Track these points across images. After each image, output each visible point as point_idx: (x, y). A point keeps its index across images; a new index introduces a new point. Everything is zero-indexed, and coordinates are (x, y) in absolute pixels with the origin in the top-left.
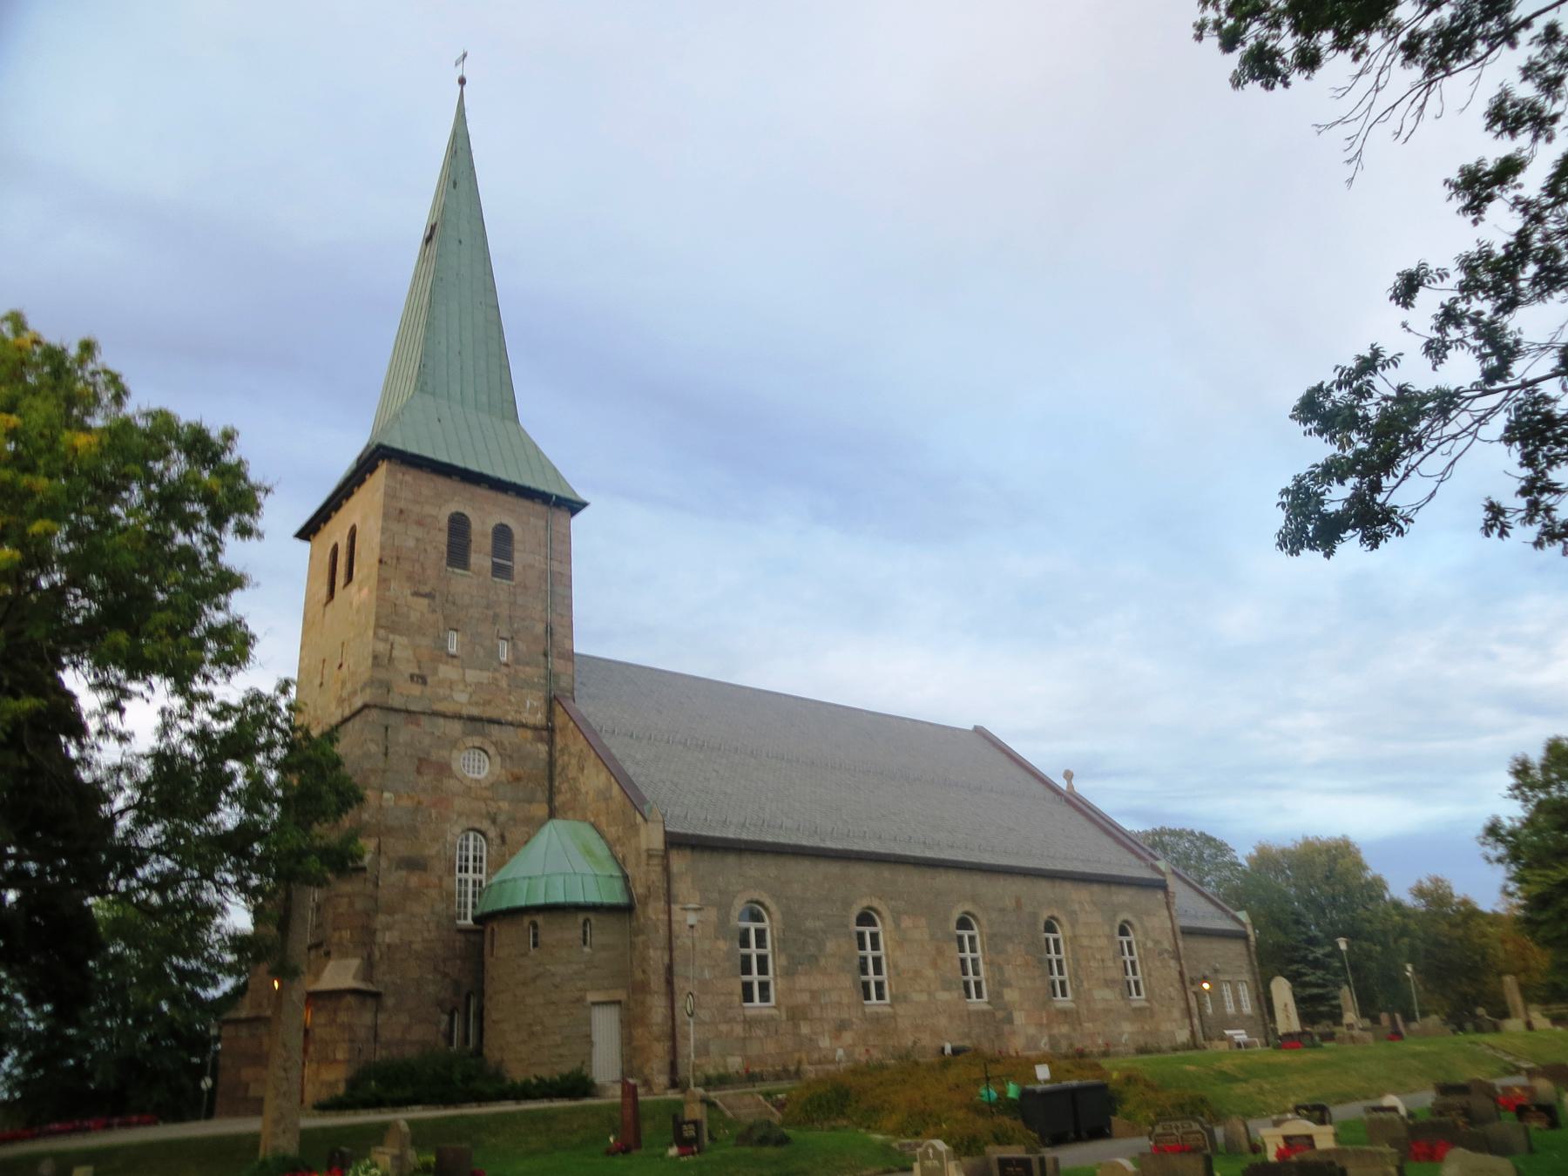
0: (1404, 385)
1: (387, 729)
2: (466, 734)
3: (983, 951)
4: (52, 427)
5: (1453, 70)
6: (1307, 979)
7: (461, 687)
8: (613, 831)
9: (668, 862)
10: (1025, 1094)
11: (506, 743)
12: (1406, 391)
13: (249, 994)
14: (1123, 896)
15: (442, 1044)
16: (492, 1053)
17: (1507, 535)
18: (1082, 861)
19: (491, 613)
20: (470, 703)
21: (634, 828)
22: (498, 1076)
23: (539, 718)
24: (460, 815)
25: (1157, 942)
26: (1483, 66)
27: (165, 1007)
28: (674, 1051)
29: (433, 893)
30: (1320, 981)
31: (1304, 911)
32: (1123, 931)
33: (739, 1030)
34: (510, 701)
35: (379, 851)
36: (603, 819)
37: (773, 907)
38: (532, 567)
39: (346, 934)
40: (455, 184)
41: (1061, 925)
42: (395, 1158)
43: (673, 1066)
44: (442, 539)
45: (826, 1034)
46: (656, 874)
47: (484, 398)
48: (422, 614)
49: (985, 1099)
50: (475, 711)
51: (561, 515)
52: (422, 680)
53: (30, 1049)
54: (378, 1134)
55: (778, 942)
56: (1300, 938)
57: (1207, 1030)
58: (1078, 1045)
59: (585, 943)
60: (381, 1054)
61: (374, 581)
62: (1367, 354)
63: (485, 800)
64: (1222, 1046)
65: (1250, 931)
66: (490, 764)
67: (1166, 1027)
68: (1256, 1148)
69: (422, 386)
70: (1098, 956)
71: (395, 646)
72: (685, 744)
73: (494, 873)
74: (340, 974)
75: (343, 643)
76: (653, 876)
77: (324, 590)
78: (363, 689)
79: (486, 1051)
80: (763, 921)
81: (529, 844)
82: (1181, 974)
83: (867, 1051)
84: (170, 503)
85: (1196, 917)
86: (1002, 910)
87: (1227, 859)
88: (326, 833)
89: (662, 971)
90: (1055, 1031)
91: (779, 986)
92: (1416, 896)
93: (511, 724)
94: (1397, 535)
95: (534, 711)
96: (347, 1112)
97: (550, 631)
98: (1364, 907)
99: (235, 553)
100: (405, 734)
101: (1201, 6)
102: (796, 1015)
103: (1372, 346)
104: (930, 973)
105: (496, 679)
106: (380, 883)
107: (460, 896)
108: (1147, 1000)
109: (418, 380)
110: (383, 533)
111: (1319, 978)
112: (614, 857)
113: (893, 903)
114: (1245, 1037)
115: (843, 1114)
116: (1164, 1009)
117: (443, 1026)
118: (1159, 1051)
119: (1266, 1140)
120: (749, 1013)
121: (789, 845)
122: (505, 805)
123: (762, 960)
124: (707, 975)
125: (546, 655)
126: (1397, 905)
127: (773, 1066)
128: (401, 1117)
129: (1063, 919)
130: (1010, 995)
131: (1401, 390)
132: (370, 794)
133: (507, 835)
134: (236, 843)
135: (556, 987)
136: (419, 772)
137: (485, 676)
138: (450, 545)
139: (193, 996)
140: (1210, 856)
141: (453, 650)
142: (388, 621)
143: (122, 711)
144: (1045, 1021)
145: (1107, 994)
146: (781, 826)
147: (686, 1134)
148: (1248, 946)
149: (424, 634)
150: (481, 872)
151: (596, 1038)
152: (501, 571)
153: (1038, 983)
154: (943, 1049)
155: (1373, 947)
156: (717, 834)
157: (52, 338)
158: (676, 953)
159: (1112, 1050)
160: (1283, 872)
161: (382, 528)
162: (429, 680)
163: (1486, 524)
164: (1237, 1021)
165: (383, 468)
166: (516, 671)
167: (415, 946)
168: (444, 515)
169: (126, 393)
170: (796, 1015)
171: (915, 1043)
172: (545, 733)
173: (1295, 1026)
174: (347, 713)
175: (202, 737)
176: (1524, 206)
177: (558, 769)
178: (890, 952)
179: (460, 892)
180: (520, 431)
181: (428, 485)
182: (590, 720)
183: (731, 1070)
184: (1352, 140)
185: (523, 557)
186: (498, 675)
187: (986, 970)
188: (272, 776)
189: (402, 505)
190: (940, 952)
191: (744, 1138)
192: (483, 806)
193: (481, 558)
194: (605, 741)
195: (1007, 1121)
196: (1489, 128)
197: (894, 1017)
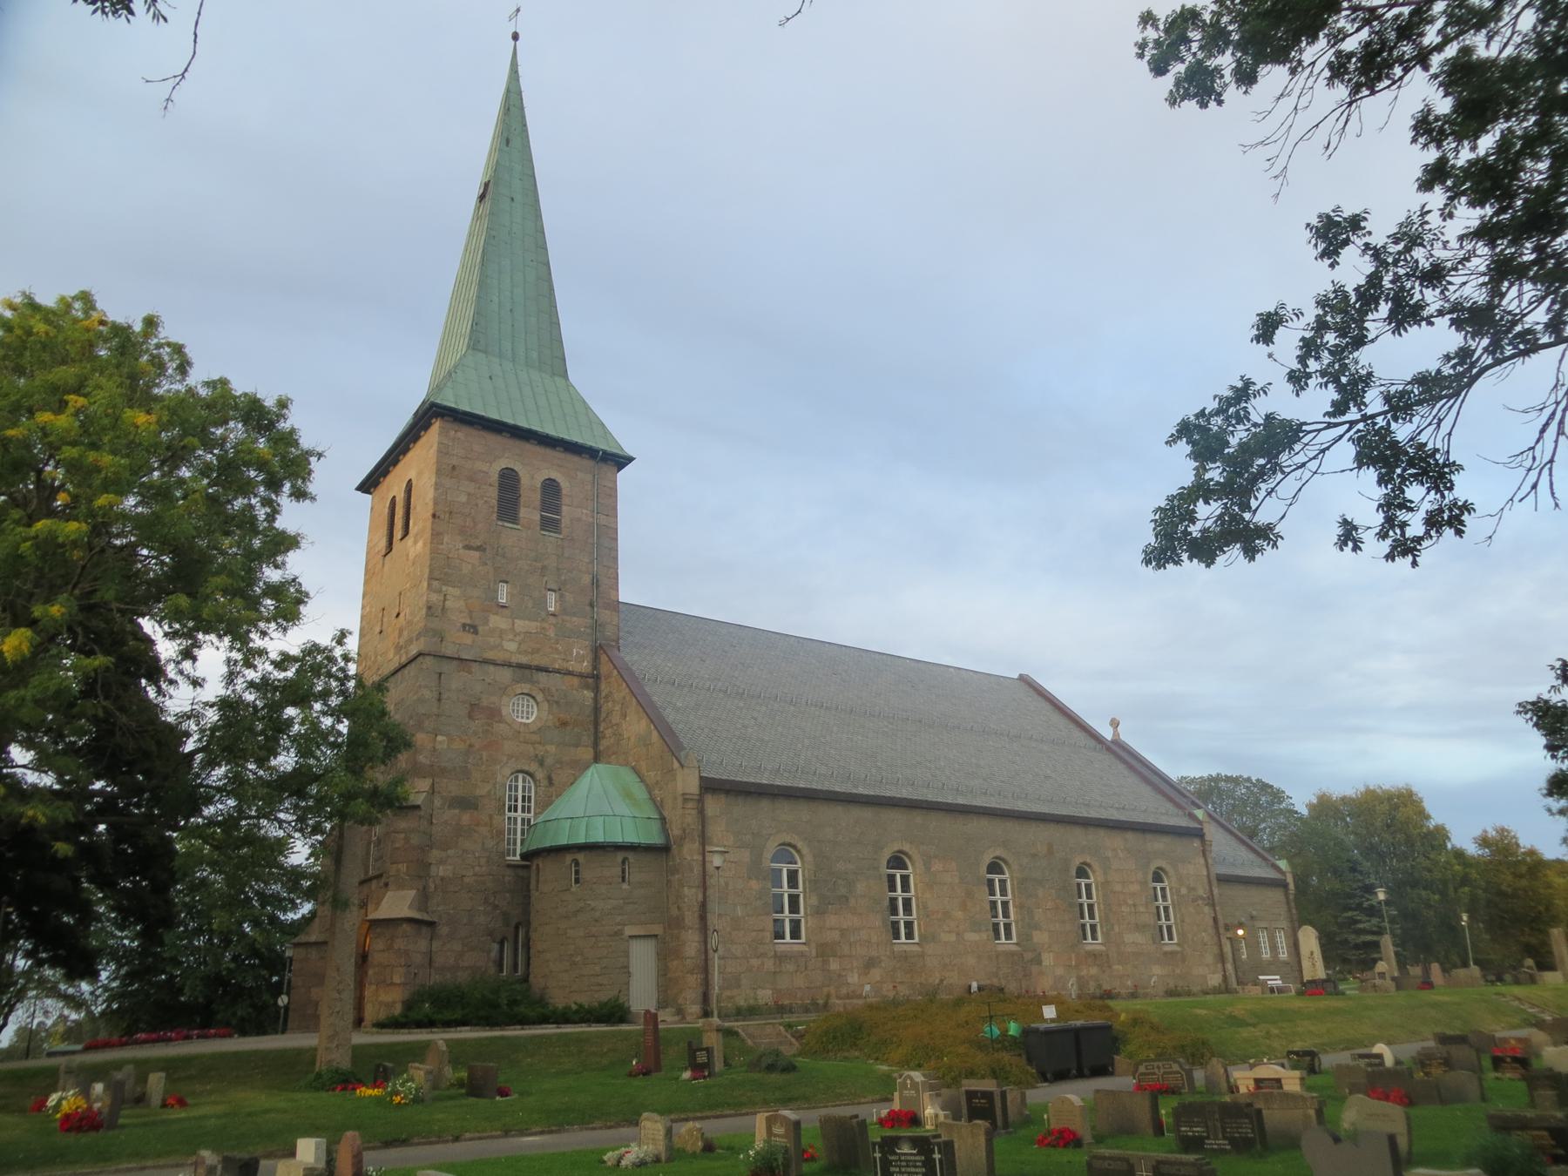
0: (1271, 414)
1: (440, 674)
4: (114, 407)
5: (1377, 89)
6: (1361, 926)
7: (511, 637)
8: (652, 776)
9: (703, 803)
10: (1026, 1032)
11: (554, 689)
12: (1274, 418)
13: (317, 920)
14: (1159, 844)
15: (492, 970)
16: (537, 981)
17: (1360, 549)
18: (1118, 809)
19: (539, 565)
22: (541, 1001)
23: (585, 666)
24: (510, 757)
25: (1191, 889)
26: (1399, 87)
27: (247, 928)
28: (706, 983)
29: (484, 830)
30: (1374, 929)
31: (1360, 858)
32: (1157, 878)
33: (769, 965)
34: (557, 649)
35: (433, 791)
36: (643, 765)
37: (805, 851)
38: (579, 520)
39: (403, 867)
41: (1094, 872)
43: (706, 998)
44: (493, 493)
45: (855, 971)
46: (691, 818)
47: (535, 355)
49: (988, 1035)
50: (524, 660)
51: (607, 469)
52: (474, 629)
54: (417, 1052)
55: (810, 882)
56: (1355, 886)
58: (1106, 987)
59: (623, 880)
60: (436, 978)
61: (428, 535)
62: (1239, 384)
66: (538, 710)
68: (1233, 1089)
69: (478, 341)
70: (1130, 902)
71: (448, 597)
72: (726, 692)
73: (540, 813)
74: (396, 904)
75: (400, 594)
77: (383, 543)
79: (531, 978)
80: (796, 863)
82: (1215, 920)
83: (894, 987)
84: (230, 474)
86: (1034, 856)
87: (1283, 805)
88: (379, 776)
89: (696, 909)
90: (1084, 973)
91: (809, 925)
92: (1480, 845)
93: (558, 672)
94: (1273, 548)
95: (580, 659)
96: (402, 1031)
97: (595, 582)
98: (1424, 856)
99: (291, 517)
100: (457, 680)
101: (1141, 27)
102: (826, 951)
103: (1242, 377)
104: (959, 914)
106: (434, 821)
107: (509, 834)
109: (470, 339)
110: (436, 489)
111: (1375, 926)
112: (652, 799)
115: (855, 1045)
117: (494, 954)
118: (1189, 994)
119: (1239, 1082)
120: (781, 948)
121: (821, 791)
122: (552, 749)
123: (794, 900)
124: (739, 912)
125: (592, 605)
126: (1459, 854)
128: (439, 1037)
129: (1096, 866)
130: (1040, 937)
131: (1269, 418)
132: (420, 738)
134: (294, 784)
136: (470, 716)
137: (533, 626)
138: (501, 500)
139: (273, 920)
140: (1267, 802)
142: (441, 572)
143: (194, 659)
145: (1139, 938)
147: (699, 1060)
148: (1287, 894)
150: (529, 812)
152: (550, 524)
154: (970, 987)
155: (1432, 895)
157: (116, 315)
158: (710, 892)
159: (1141, 991)
160: (1343, 820)
161: (436, 484)
162: (480, 629)
163: (1339, 539)
164: (1273, 966)
165: (436, 426)
166: (563, 621)
167: (466, 880)
169: (189, 364)
170: (826, 951)
171: (942, 981)
172: (590, 681)
173: (1321, 973)
174: (404, 660)
175: (263, 686)
176: (1377, 254)
177: (603, 715)
178: (920, 895)
179: (509, 829)
180: (569, 385)
183: (761, 1002)
184: (1272, 161)
186: (546, 625)
187: (1016, 913)
189: (454, 461)
191: (753, 1066)
193: (530, 512)
194: (647, 689)
195: (1006, 1057)
196: (1414, 141)
197: (922, 955)
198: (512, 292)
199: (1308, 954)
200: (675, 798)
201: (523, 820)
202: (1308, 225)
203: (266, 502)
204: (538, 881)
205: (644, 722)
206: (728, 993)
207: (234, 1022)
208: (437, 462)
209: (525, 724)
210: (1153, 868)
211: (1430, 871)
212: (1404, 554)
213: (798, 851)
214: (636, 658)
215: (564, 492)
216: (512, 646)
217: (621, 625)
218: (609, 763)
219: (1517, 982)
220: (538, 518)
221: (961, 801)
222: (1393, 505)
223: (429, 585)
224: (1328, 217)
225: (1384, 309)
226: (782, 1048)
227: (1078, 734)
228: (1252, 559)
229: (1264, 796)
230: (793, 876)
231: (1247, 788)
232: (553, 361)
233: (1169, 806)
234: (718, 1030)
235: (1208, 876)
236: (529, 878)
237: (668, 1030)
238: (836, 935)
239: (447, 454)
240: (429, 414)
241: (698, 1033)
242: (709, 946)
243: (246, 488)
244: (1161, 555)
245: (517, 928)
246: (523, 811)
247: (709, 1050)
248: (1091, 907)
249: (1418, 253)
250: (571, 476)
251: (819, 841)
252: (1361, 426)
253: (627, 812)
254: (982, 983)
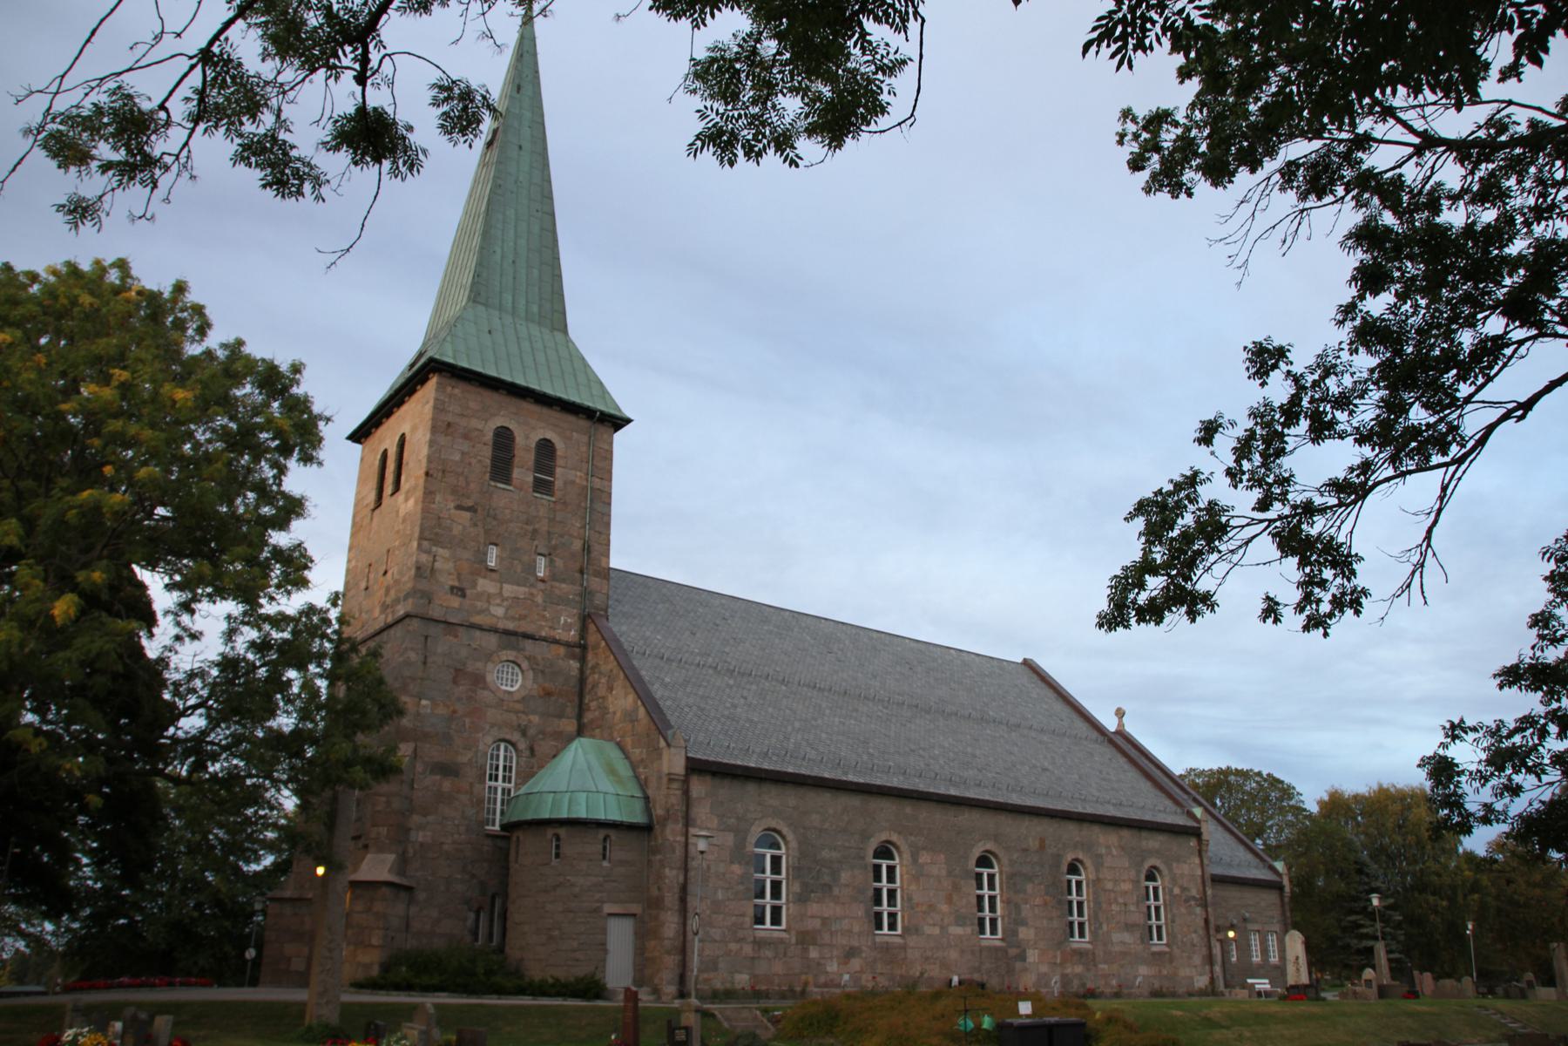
1: (426, 637)
2: (502, 647)
3: (1001, 889)
6: (1364, 931)
7: (498, 601)
8: (637, 753)
10: (1001, 1027)
11: (539, 657)
14: (1154, 842)
15: (468, 938)
16: (513, 952)
19: (530, 528)
21: (657, 753)
22: (517, 973)
23: (572, 635)
24: (493, 725)
25: (1183, 889)
27: (210, 877)
28: (684, 965)
33: (748, 949)
34: (544, 616)
36: (628, 740)
37: (790, 836)
38: (573, 482)
39: (384, 830)
40: (519, 88)
41: (1085, 868)
42: (422, 1032)
43: (682, 979)
44: (487, 453)
47: (535, 309)
48: (464, 527)
49: (962, 1028)
50: (511, 626)
51: (603, 430)
52: (460, 591)
53: (88, 905)
54: (409, 1012)
55: (794, 868)
56: (1361, 888)
57: (1228, 977)
58: (1090, 985)
59: (604, 857)
61: (419, 493)
62: (1189, 473)
63: (517, 712)
64: (1242, 994)
65: (1286, 882)
67: (1185, 972)
69: (479, 293)
70: (1121, 900)
73: (524, 783)
74: (376, 867)
76: (673, 800)
77: (372, 496)
78: (406, 598)
79: (507, 949)
81: (557, 759)
82: (1207, 921)
85: (1230, 865)
86: (1025, 850)
87: (1292, 802)
89: (676, 890)
90: (1069, 971)
93: (544, 639)
95: (567, 627)
97: (587, 548)
99: (297, 480)
100: (443, 644)
102: (806, 939)
104: (944, 908)
105: (532, 594)
107: (489, 803)
112: (637, 777)
113: (913, 838)
114: (1268, 986)
116: (1185, 954)
117: (470, 922)
118: (1174, 995)
121: (809, 777)
122: (535, 719)
123: (776, 886)
124: (720, 895)
125: (582, 572)
127: (779, 985)
128: (429, 1001)
129: (1088, 863)
130: (1025, 933)
133: (536, 748)
135: (575, 896)
136: (455, 682)
137: (521, 591)
138: (494, 459)
141: (492, 564)
142: (432, 532)
144: (1058, 961)
145: (1127, 937)
146: (804, 759)
149: (465, 548)
150: (510, 782)
151: (610, 946)
152: (542, 486)
153: (1055, 924)
154: (951, 981)
156: (739, 763)
157: (150, 284)
158: (691, 874)
159: (1125, 991)
160: (1355, 819)
162: (468, 592)
165: (433, 381)
167: (446, 847)
169: (209, 326)
170: (806, 939)
171: (922, 974)
174: (390, 619)
176: (1297, 379)
180: (568, 341)
181: (475, 398)
182: (622, 639)
183: (738, 987)
186: (534, 591)
187: (1002, 909)
188: (322, 684)
189: (450, 418)
190: (956, 888)
192: (514, 718)
193: (523, 474)
194: (635, 662)
197: (904, 947)
198: (515, 244)
199: (1293, 959)
200: (660, 778)
201: (503, 790)
202: (1245, 348)
203: (275, 465)
204: (517, 853)
205: (631, 697)
206: (706, 975)
207: (58, 989)
208: (433, 419)
209: (509, 693)
210: (1146, 866)
211: (1439, 875)
212: (1316, 626)
213: (783, 837)
214: (624, 628)
215: (559, 453)
216: (500, 611)
217: (611, 593)
218: (593, 737)
219: (1507, 996)
220: (530, 479)
221: (953, 792)
222: (1310, 583)
223: (419, 545)
224: (1261, 344)
225: (1304, 424)
226: (758, 1032)
227: (1080, 724)
228: (1193, 620)
229: (1274, 792)
230: (776, 861)
231: (1257, 782)
232: (554, 315)
233: (1168, 803)
234: (697, 1011)
235: (1203, 876)
236: (508, 850)
237: (646, 1008)
238: (817, 923)
239: (443, 410)
240: (424, 371)
241: (678, 1012)
242: (689, 928)
243: (258, 452)
244: (1114, 619)
245: (493, 897)
246: (504, 781)
247: (687, 1029)
248: (1080, 904)
249: (1331, 382)
250: (565, 436)
251: (804, 828)
252: (1278, 524)
253: (611, 789)
254: (963, 977)
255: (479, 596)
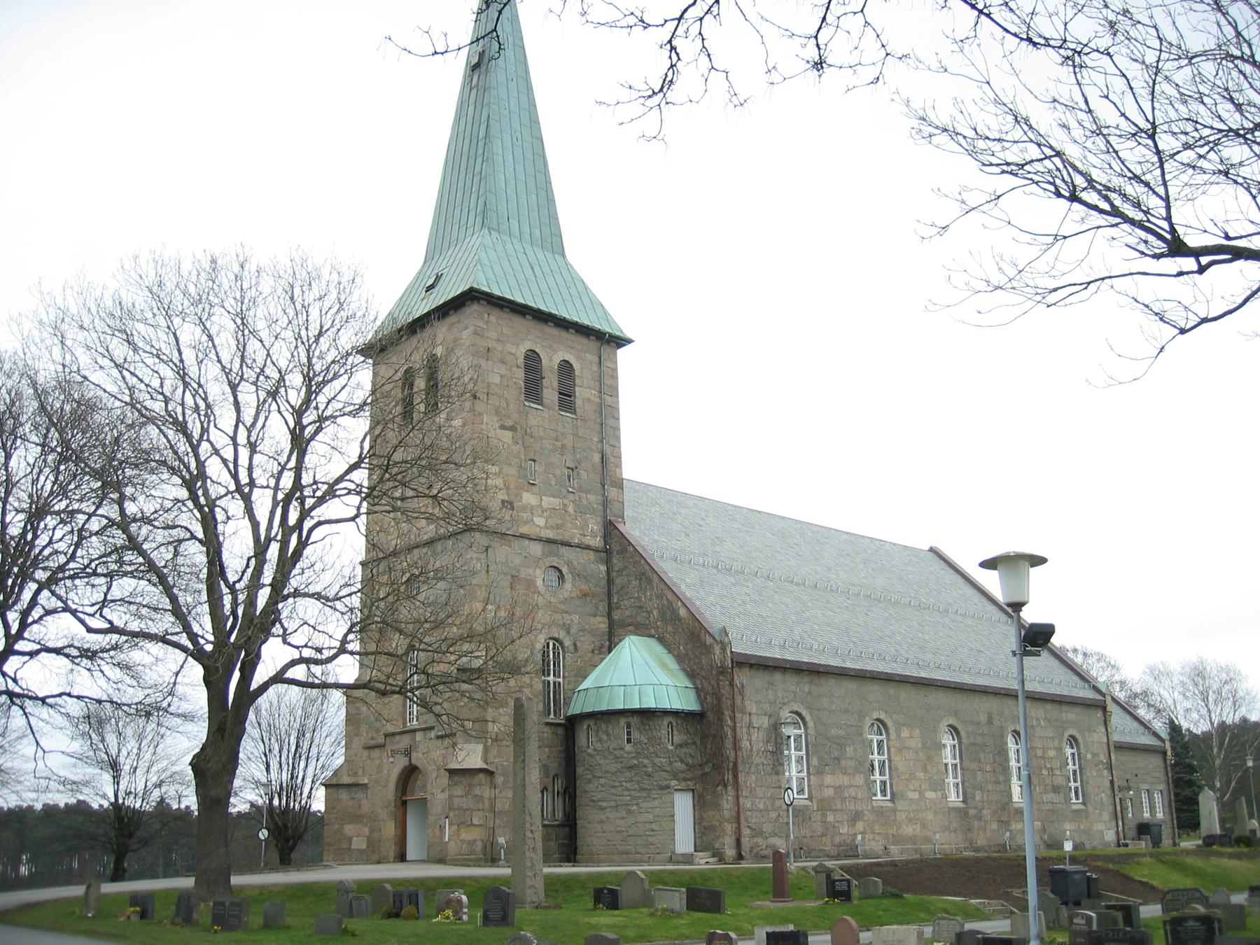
2: (545, 555)
11: (575, 563)
14: (1070, 714)
19: (559, 444)
20: (546, 527)
25: (1095, 755)
34: (576, 524)
38: (589, 400)
44: (520, 374)
50: (550, 534)
51: (606, 350)
82: (1112, 782)
93: (578, 546)
104: (920, 775)
105: (565, 505)
108: (1084, 803)
133: (579, 644)
137: (556, 502)
138: (526, 381)
149: (510, 465)
162: (515, 505)
168: (521, 351)
185: (584, 392)
186: (566, 501)
193: (550, 393)
232: (552, 241)
238: (829, 792)
255: (524, 508)
